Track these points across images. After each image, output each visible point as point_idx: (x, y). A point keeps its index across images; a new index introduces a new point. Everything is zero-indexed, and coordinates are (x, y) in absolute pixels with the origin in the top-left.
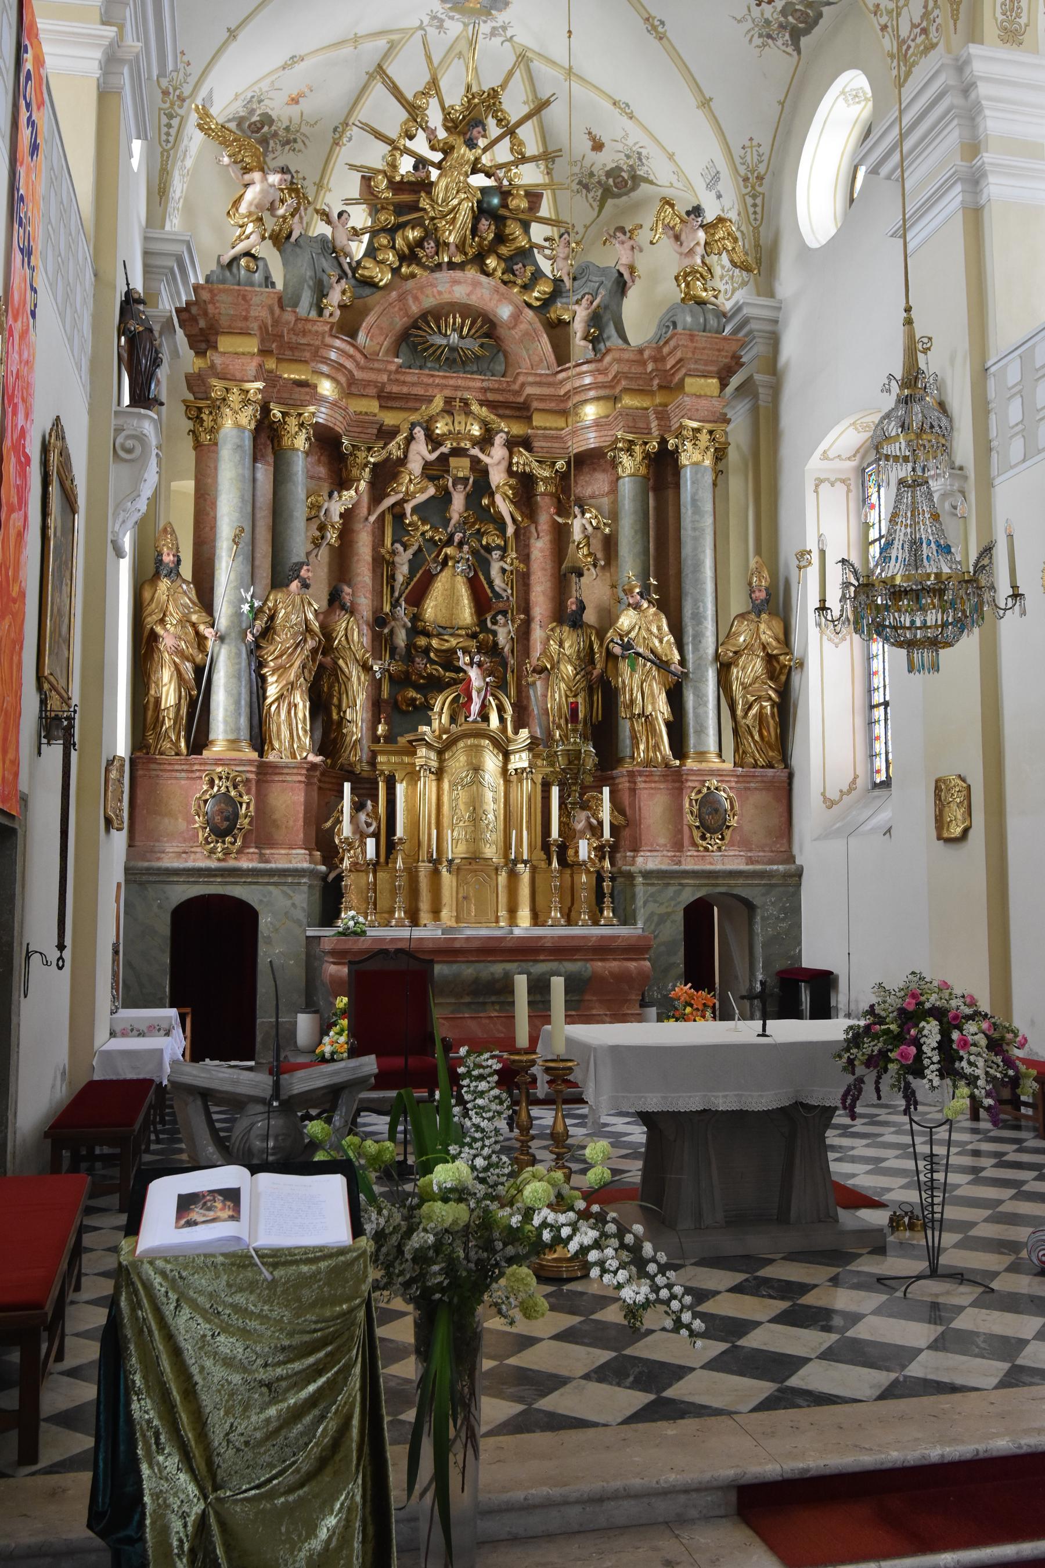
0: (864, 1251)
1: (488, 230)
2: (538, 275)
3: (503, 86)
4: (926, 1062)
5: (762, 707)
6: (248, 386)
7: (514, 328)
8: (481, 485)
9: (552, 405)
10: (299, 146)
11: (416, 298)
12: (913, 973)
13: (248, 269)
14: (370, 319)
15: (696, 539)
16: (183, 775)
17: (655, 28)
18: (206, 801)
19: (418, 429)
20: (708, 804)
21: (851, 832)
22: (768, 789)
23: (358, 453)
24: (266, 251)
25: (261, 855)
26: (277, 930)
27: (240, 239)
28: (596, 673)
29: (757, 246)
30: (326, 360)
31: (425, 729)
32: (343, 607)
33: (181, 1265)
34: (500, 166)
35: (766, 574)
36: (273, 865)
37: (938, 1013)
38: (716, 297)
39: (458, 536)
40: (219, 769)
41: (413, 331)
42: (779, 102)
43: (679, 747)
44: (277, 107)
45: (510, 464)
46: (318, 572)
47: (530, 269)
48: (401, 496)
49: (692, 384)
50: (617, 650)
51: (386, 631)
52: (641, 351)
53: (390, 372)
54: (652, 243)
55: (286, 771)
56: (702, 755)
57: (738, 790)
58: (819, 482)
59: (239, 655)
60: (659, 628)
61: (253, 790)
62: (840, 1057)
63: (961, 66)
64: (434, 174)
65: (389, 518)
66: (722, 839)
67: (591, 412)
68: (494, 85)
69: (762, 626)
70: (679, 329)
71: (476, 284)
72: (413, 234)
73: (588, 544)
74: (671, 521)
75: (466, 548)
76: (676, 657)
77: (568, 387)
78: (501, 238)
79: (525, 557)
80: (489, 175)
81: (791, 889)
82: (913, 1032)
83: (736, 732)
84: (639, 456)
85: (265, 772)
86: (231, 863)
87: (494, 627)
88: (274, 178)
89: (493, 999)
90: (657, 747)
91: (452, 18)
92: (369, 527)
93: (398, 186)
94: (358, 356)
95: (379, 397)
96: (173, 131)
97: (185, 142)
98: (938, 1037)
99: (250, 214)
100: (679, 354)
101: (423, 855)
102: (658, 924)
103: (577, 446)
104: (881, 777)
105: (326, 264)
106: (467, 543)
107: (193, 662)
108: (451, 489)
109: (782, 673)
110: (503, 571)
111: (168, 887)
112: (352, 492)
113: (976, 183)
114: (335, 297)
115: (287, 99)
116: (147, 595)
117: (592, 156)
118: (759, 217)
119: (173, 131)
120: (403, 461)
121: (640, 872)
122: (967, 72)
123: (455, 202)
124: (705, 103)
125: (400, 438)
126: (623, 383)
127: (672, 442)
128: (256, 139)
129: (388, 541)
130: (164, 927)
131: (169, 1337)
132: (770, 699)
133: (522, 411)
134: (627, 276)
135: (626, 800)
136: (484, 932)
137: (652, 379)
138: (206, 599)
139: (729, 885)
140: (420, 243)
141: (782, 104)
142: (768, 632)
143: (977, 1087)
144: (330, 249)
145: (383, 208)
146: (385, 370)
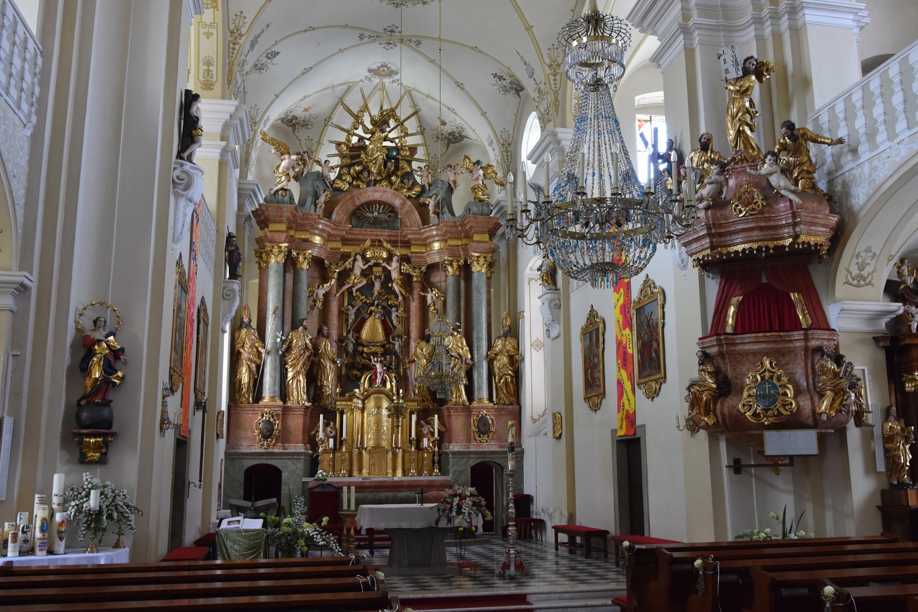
1: (391, 166)
2: (415, 183)
5: (506, 379)
9: (420, 242)
20: (483, 421)
27: (279, 183)
31: (357, 390)
32: (323, 336)
33: (227, 532)
39: (376, 302)
43: (470, 397)
44: (299, 113)
46: (312, 322)
56: (480, 400)
57: (496, 416)
58: (530, 279)
59: (276, 360)
64: (367, 142)
67: (436, 246)
71: (384, 192)
72: (357, 168)
76: (470, 356)
79: (407, 310)
85: (286, 410)
86: (270, 450)
88: (294, 157)
90: (460, 396)
93: (352, 148)
100: (470, 224)
101: (355, 446)
103: (430, 261)
105: (318, 184)
109: (516, 363)
110: (397, 316)
114: (322, 199)
116: (237, 335)
120: (352, 270)
124: (484, 114)
125: (350, 260)
129: (346, 304)
130: (241, 478)
131: (225, 545)
133: (407, 244)
135: (446, 419)
140: (361, 172)
142: (510, 344)
144: (321, 177)
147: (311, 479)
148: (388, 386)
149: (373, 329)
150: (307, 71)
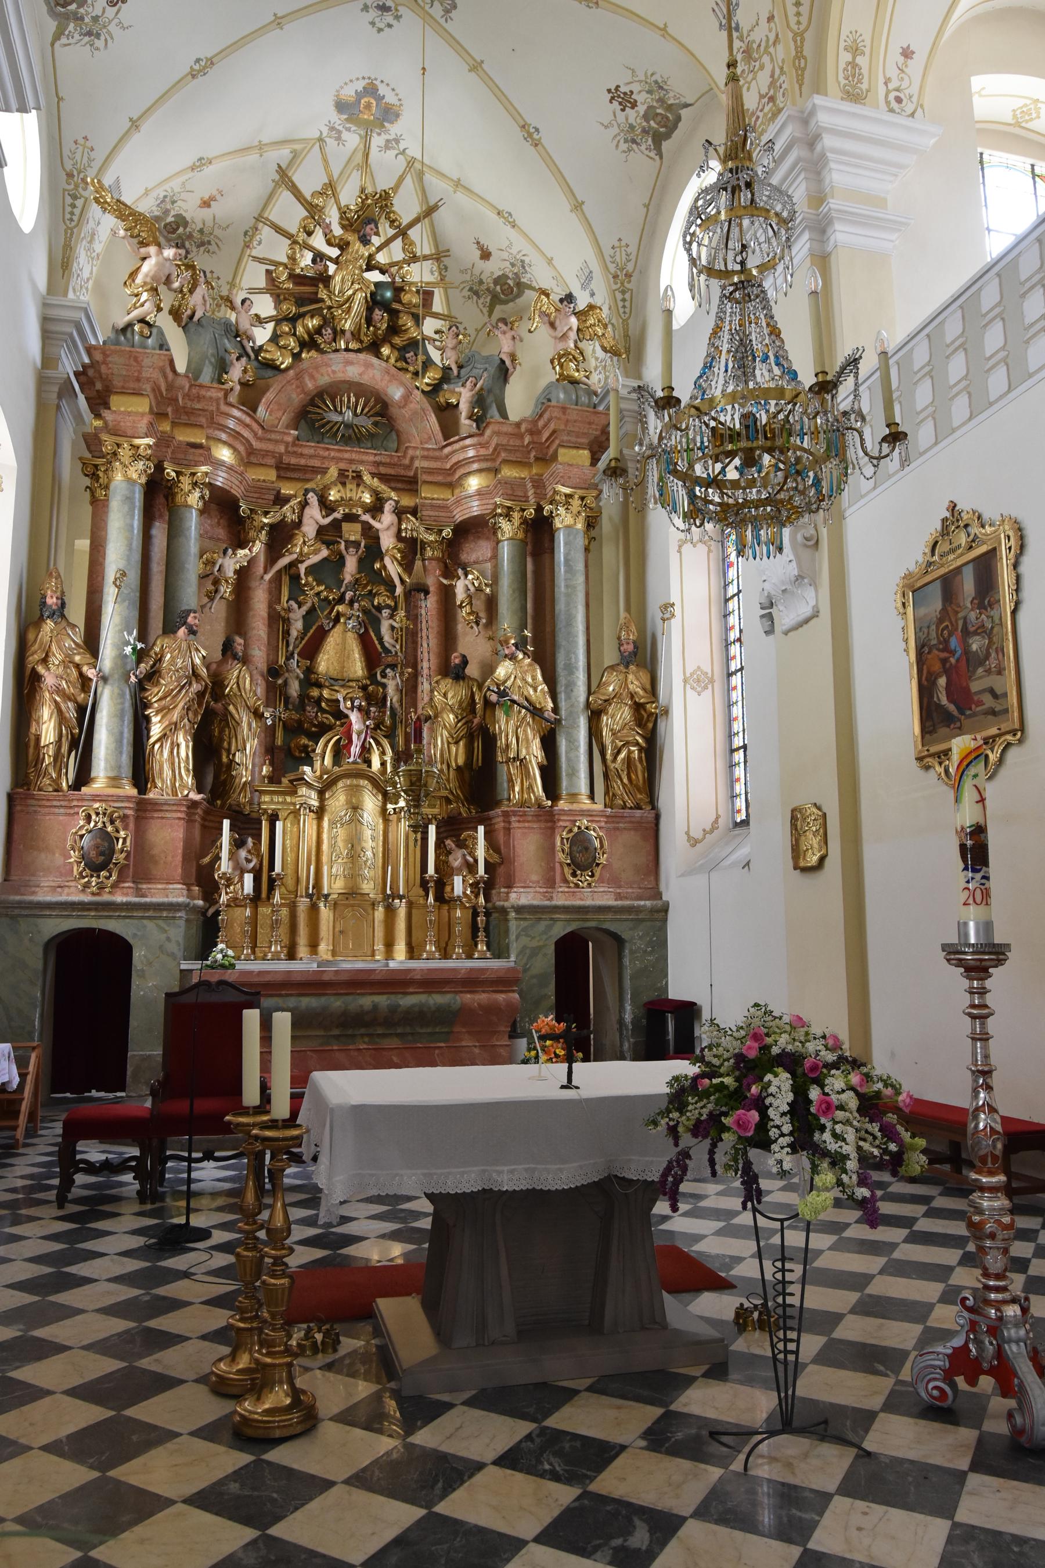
0: (696, 1371)
2: (428, 363)
3: (396, 188)
4: (773, 1133)
5: (630, 752)
6: (137, 442)
7: (404, 407)
8: (373, 551)
9: (439, 478)
10: (213, 248)
11: (312, 377)
12: (756, 1005)
13: (141, 334)
14: (270, 395)
15: (568, 595)
16: (62, 810)
17: (530, 135)
18: (82, 836)
19: (311, 495)
20: (579, 842)
21: (713, 867)
22: (635, 829)
23: (256, 517)
24: (165, 322)
25: (138, 890)
26: (150, 964)
28: (476, 721)
29: (626, 336)
30: (223, 428)
31: (307, 769)
32: (235, 657)
34: (393, 264)
35: (633, 628)
36: (148, 900)
37: (791, 1061)
38: (587, 377)
39: (349, 595)
40: (96, 805)
41: (310, 408)
42: (644, 205)
44: (189, 208)
45: (399, 531)
46: (214, 621)
47: (421, 358)
48: (295, 556)
49: (565, 455)
50: (494, 698)
51: (280, 681)
52: (518, 425)
53: (287, 444)
54: (530, 331)
55: (165, 808)
56: (573, 797)
57: (608, 831)
59: (122, 695)
60: (534, 678)
61: (132, 826)
62: (655, 1123)
63: (805, 119)
64: (332, 268)
65: (285, 579)
66: (592, 876)
67: (474, 483)
68: (386, 188)
69: (631, 677)
70: (554, 403)
71: (368, 365)
73: (470, 603)
74: (548, 584)
75: (356, 605)
76: (551, 705)
77: (454, 459)
78: (394, 329)
79: (413, 616)
80: (383, 272)
81: (658, 924)
82: (755, 1089)
83: (606, 776)
84: (517, 521)
86: (106, 897)
87: (384, 680)
88: (169, 253)
89: (363, 1031)
90: (531, 788)
91: (348, 130)
92: (265, 585)
93: (298, 279)
94: (255, 426)
95: (278, 468)
96: (77, 211)
97: (92, 224)
98: (790, 1097)
99: (145, 283)
100: (552, 426)
102: (531, 957)
103: (459, 516)
104: (741, 817)
106: (358, 601)
107: (76, 702)
108: (344, 552)
109: (649, 720)
110: (393, 628)
111: (40, 921)
112: (247, 551)
113: (823, 231)
115: (199, 202)
116: (31, 636)
117: (482, 265)
118: (627, 310)
119: (77, 211)
120: (299, 524)
121: (513, 907)
122: (812, 124)
123: (350, 292)
124: (578, 206)
126: (503, 455)
127: (547, 508)
128: (166, 229)
132: (637, 744)
134: (508, 363)
135: (501, 837)
136: (360, 965)
137: (529, 452)
138: (92, 643)
139: (599, 920)
140: (318, 331)
141: (647, 206)
142: (636, 682)
143: (845, 1171)
144: (236, 333)
145: (285, 299)
146: (282, 441)
147: (196, 965)
148: (376, 764)
149: (343, 655)
150: (201, 68)
